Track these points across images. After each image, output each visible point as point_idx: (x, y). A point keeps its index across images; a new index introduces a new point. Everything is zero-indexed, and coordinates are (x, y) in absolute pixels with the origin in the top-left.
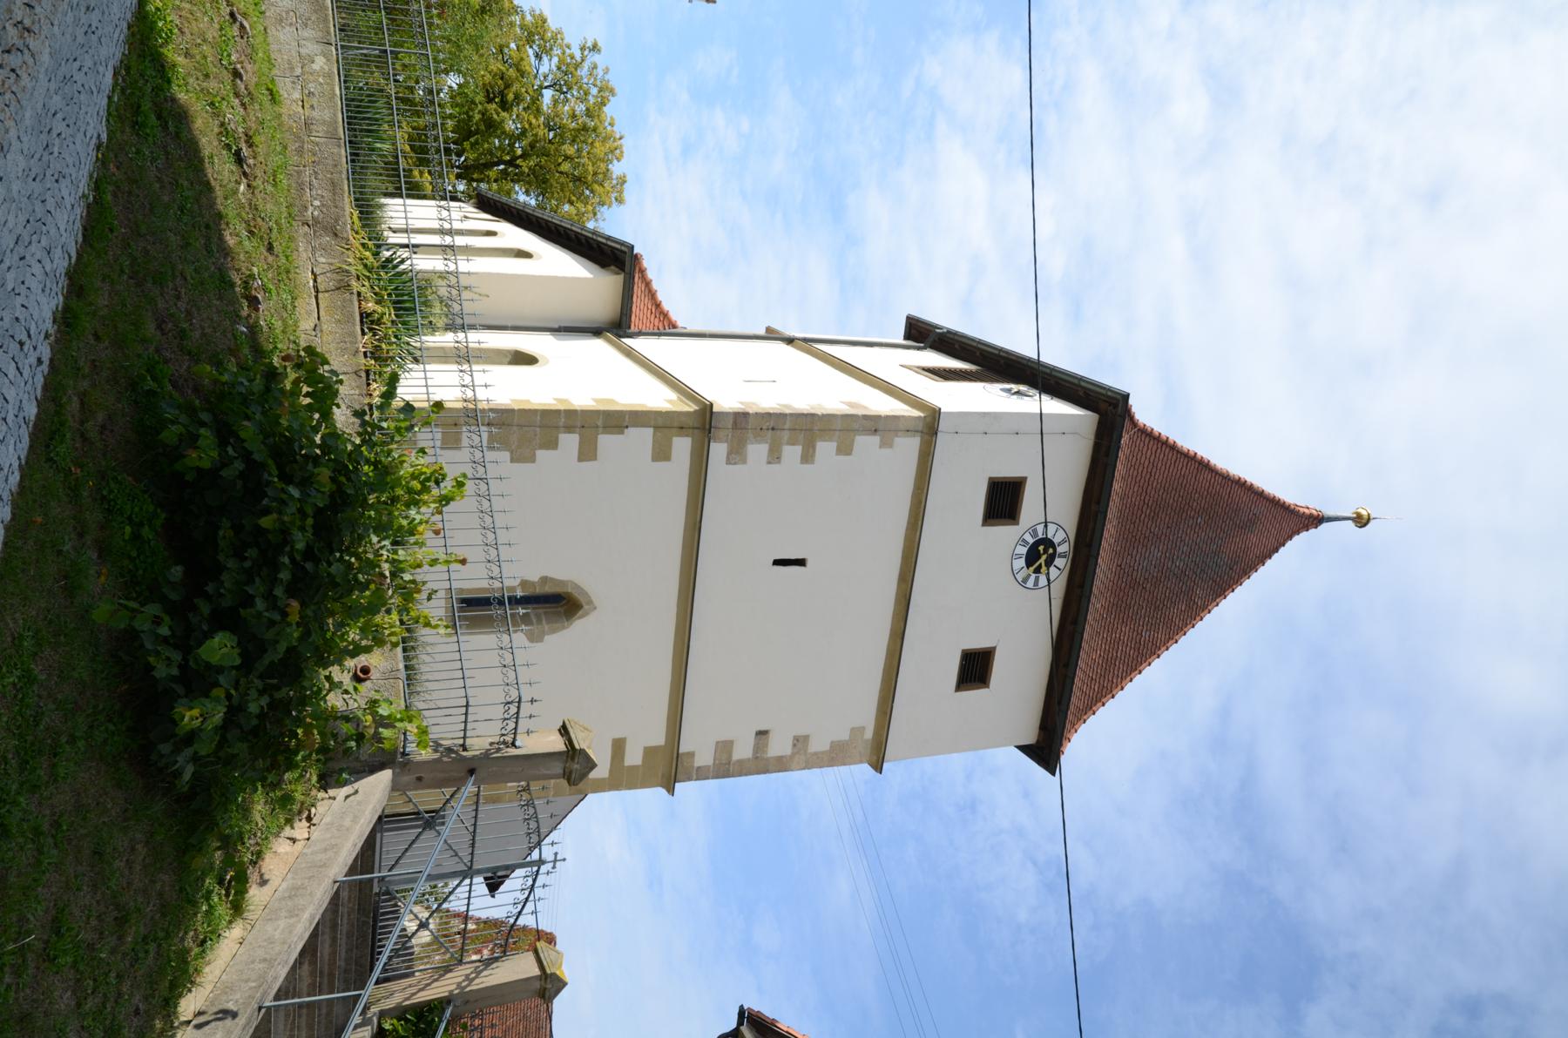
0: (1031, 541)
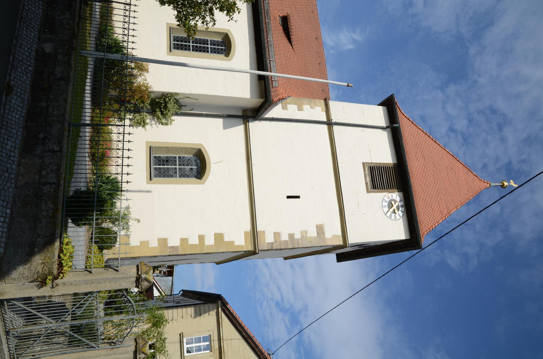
0: (388, 200)
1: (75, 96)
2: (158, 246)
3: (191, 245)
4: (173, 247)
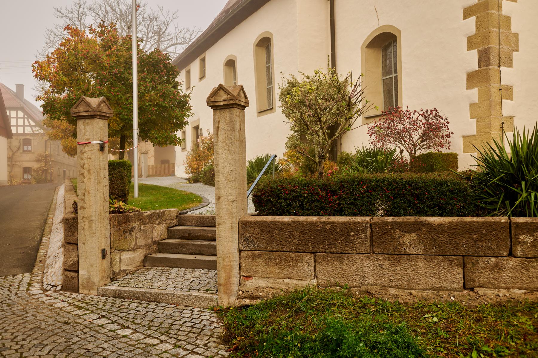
2: (477, 87)
4: (479, 61)
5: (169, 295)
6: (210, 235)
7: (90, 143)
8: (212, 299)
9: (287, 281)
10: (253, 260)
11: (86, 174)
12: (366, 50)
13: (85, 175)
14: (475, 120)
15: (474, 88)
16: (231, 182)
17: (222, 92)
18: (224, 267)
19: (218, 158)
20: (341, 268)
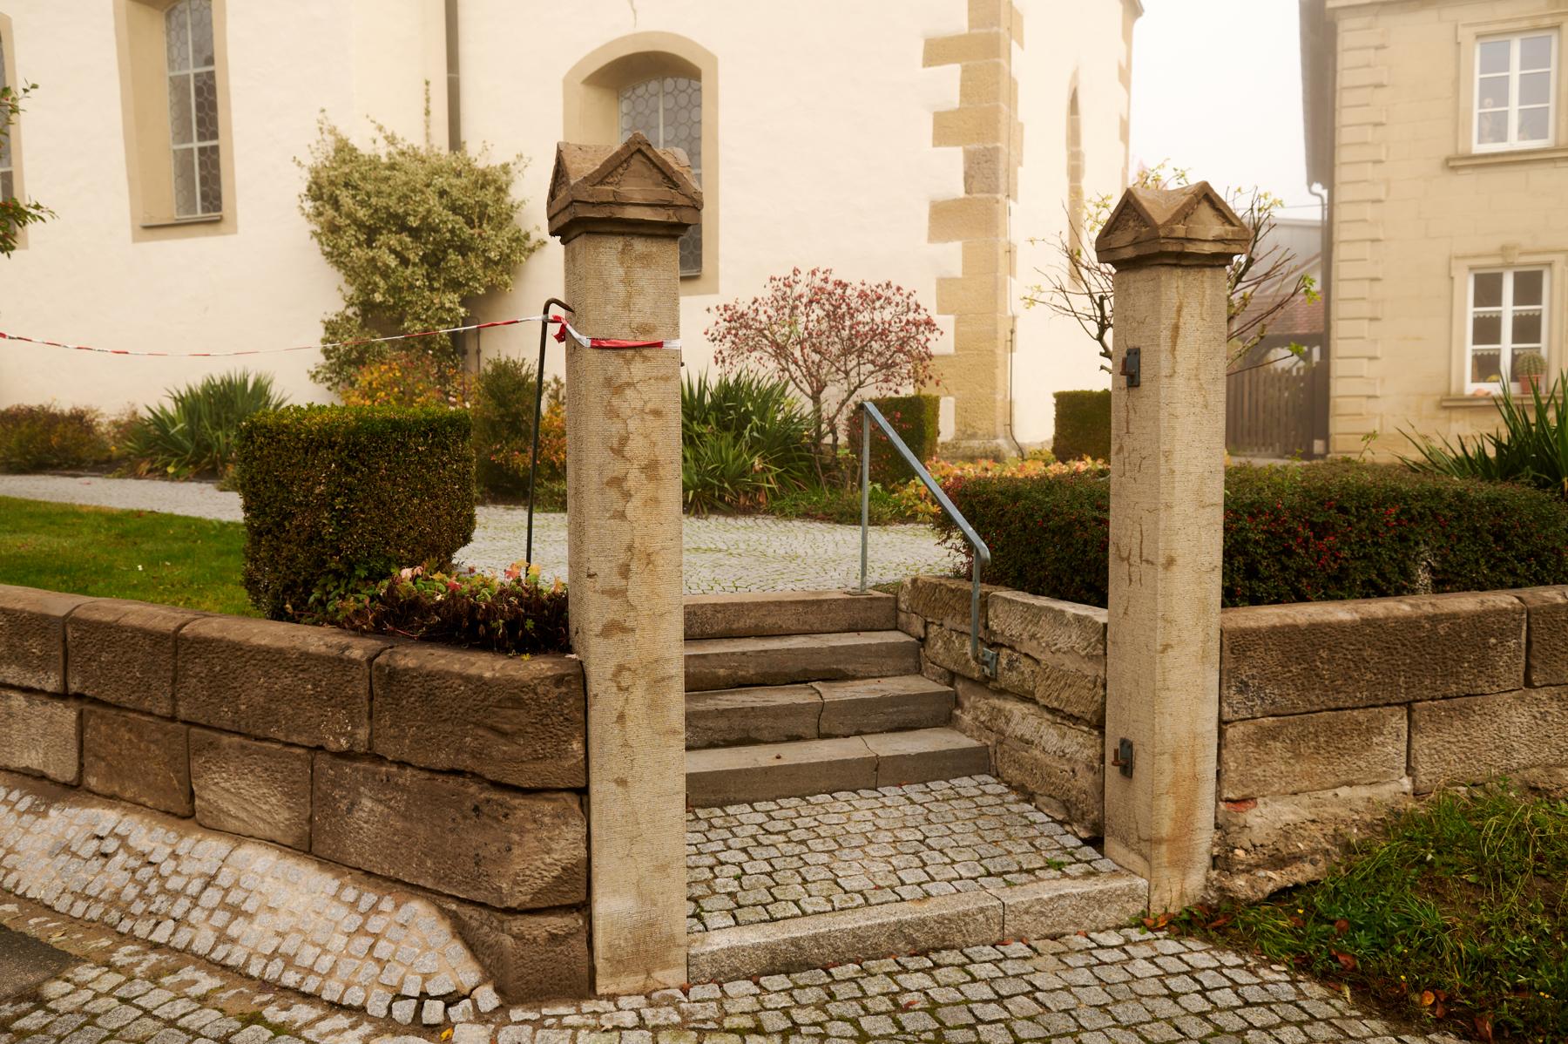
1: (287, 736)
2: (959, 238)
3: (964, 94)
4: (968, 178)
5: (990, 913)
6: (722, 672)
7: (660, 345)
8: (1132, 895)
9: (1344, 792)
10: (1258, 747)
11: (634, 478)
12: (582, 89)
13: (630, 484)
14: (951, 318)
15: (949, 239)
16: (1209, 510)
17: (1205, 211)
18: (1175, 784)
19: (1173, 428)
20: (1466, 735)
